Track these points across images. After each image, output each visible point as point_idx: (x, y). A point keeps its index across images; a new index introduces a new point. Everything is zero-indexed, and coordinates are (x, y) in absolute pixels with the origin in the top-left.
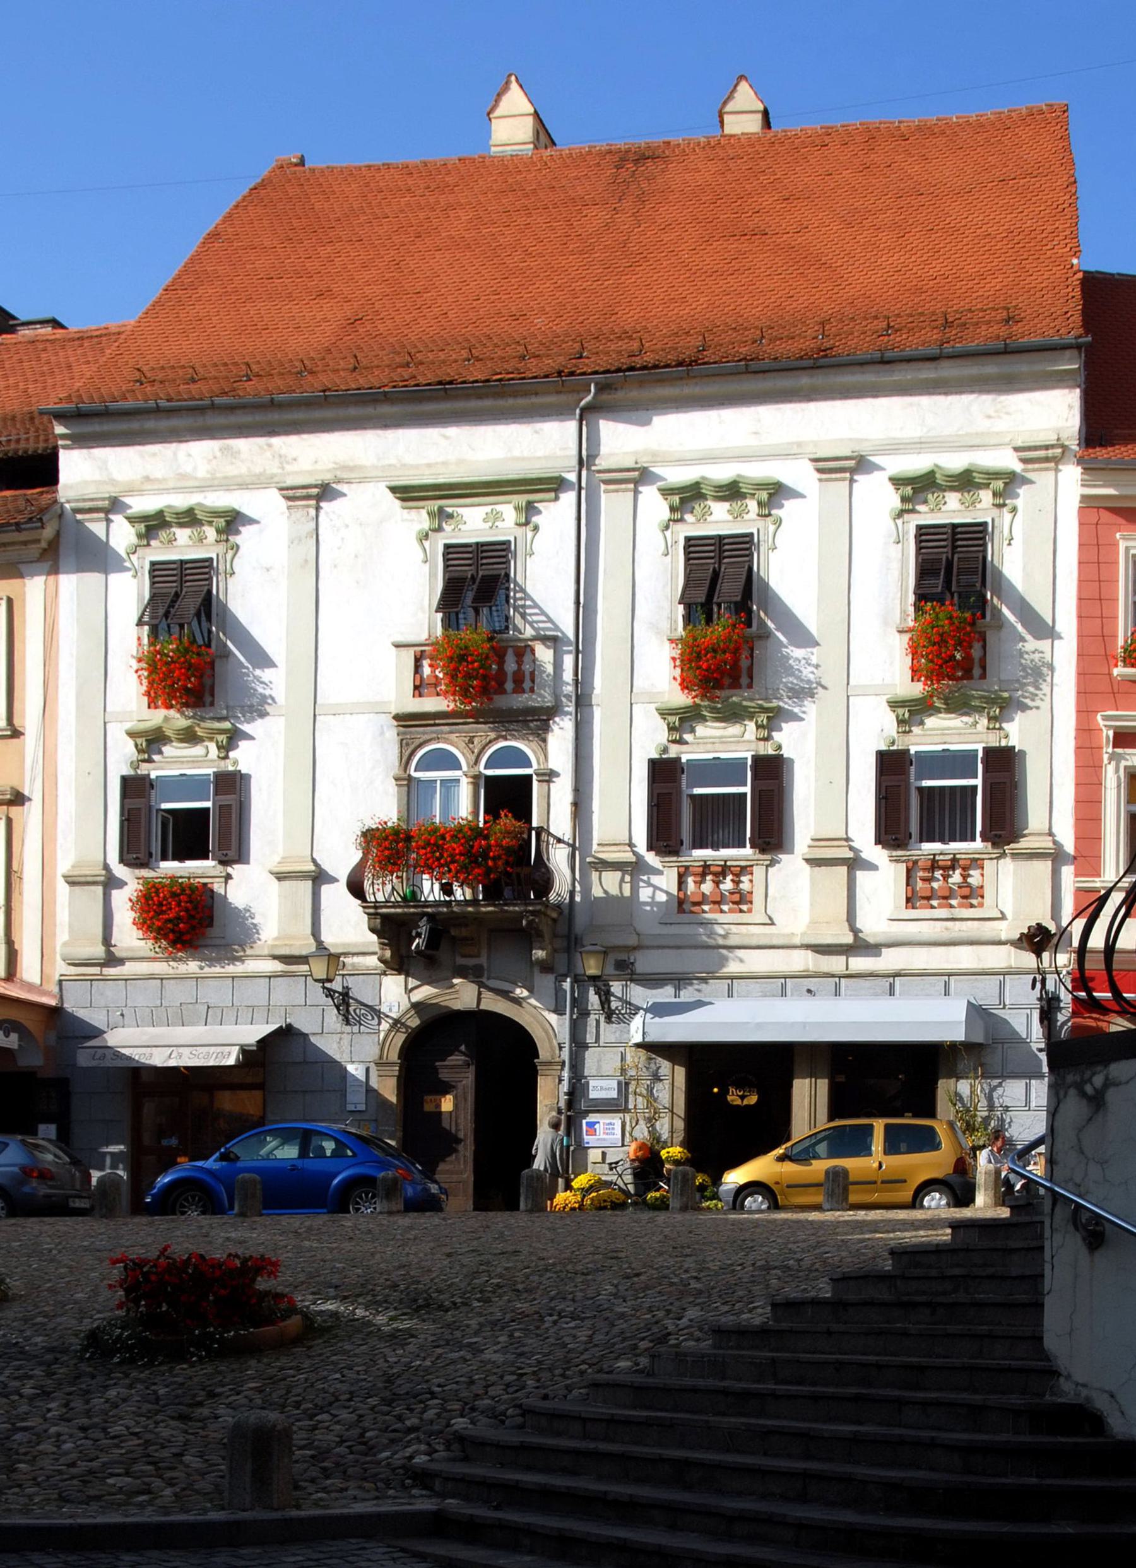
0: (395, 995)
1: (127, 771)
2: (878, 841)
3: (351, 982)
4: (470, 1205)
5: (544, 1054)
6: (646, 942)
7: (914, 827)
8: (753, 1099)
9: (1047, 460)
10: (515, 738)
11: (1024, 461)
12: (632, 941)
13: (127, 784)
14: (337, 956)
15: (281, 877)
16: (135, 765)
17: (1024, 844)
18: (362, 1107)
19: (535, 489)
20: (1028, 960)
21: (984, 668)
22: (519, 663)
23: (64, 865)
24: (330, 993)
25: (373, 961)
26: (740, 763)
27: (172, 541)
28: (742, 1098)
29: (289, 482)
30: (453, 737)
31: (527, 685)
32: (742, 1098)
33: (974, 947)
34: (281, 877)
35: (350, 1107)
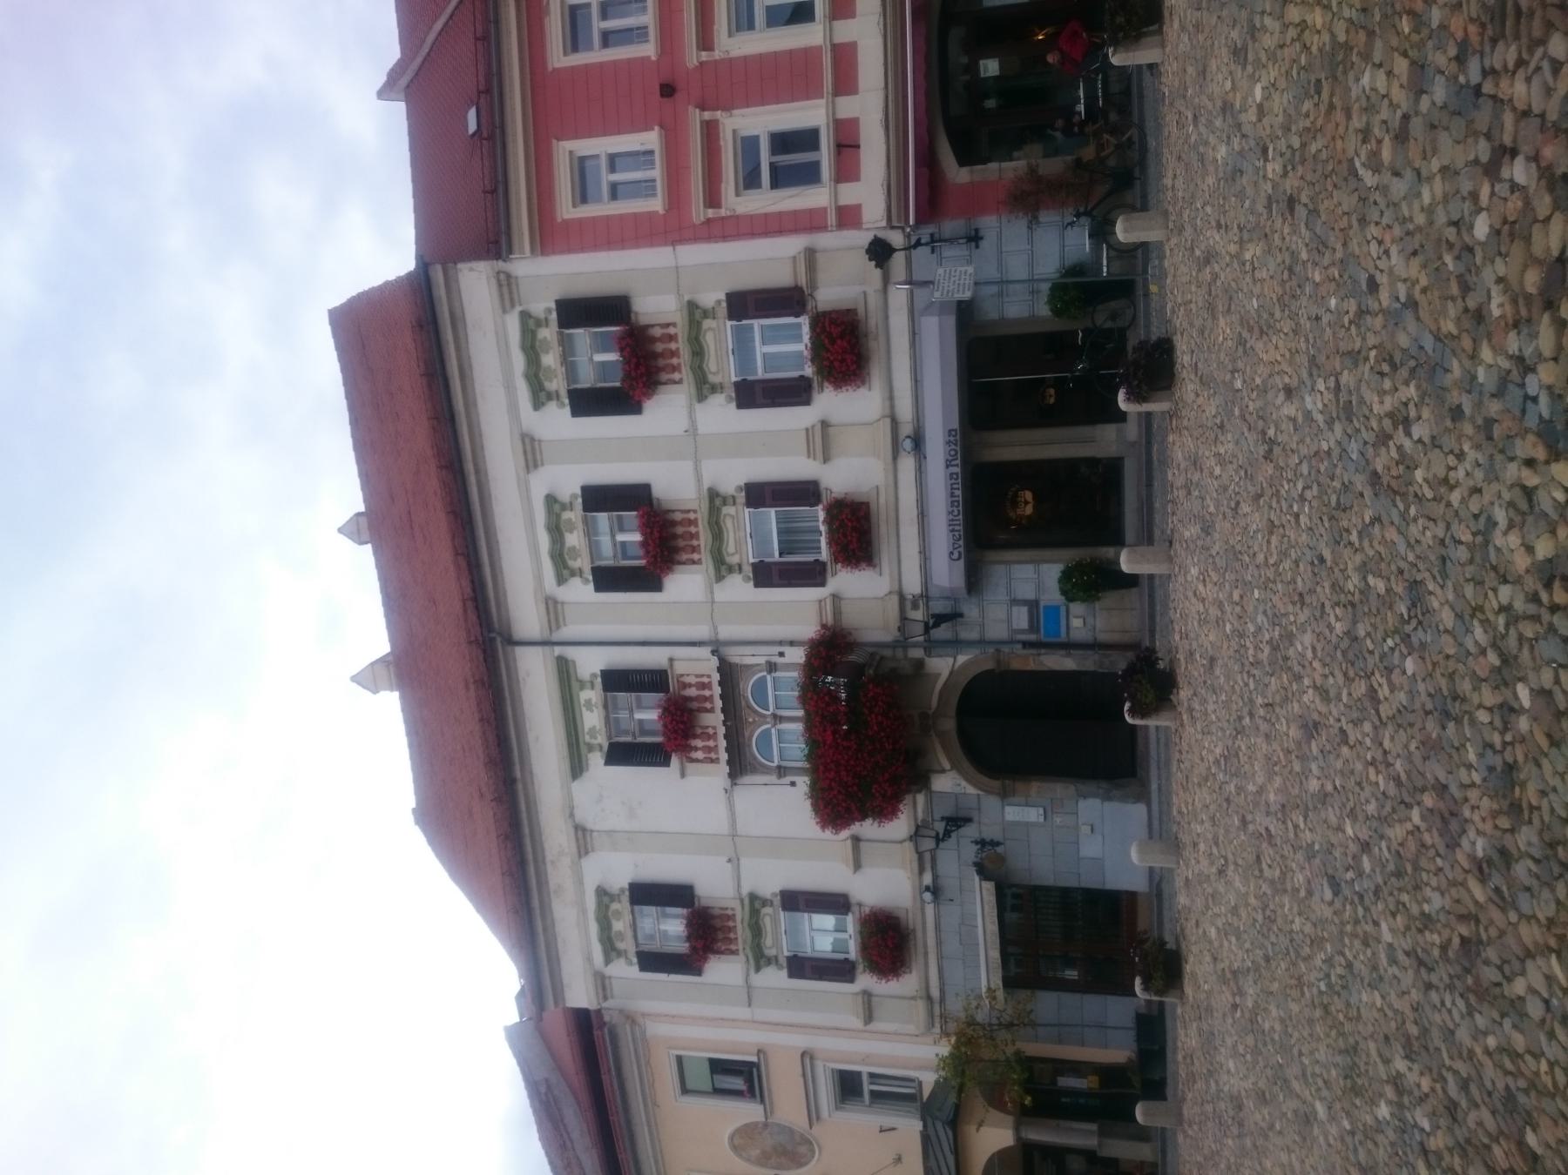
0: (948, 782)
1: (784, 973)
2: (807, 402)
3: (937, 816)
4: (1134, 590)
5: (989, 665)
6: (896, 588)
7: (810, 558)
8: (1028, 495)
9: (509, 285)
10: (750, 746)
11: (513, 306)
12: (895, 599)
13: (759, 583)
14: (918, 827)
15: (857, 865)
16: (780, 967)
17: (803, 281)
18: (1041, 811)
19: (564, 670)
20: (898, 260)
21: (668, 325)
22: (690, 685)
23: (857, 1023)
24: (947, 834)
25: (921, 798)
26: (736, 330)
27: (620, 934)
28: (1026, 503)
29: (574, 850)
30: (747, 734)
31: (706, 680)
32: (1026, 503)
33: (891, 313)
34: (857, 865)
35: (1042, 819)
